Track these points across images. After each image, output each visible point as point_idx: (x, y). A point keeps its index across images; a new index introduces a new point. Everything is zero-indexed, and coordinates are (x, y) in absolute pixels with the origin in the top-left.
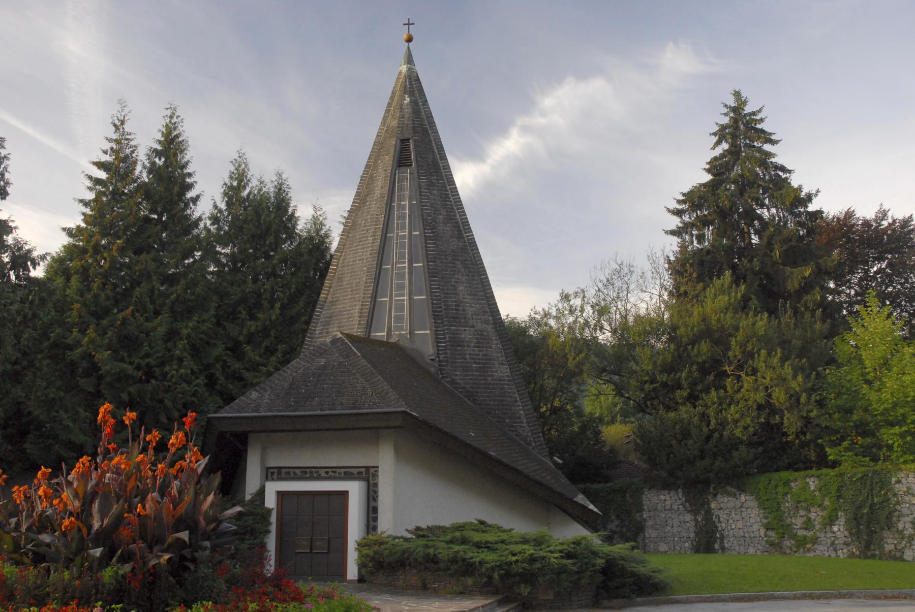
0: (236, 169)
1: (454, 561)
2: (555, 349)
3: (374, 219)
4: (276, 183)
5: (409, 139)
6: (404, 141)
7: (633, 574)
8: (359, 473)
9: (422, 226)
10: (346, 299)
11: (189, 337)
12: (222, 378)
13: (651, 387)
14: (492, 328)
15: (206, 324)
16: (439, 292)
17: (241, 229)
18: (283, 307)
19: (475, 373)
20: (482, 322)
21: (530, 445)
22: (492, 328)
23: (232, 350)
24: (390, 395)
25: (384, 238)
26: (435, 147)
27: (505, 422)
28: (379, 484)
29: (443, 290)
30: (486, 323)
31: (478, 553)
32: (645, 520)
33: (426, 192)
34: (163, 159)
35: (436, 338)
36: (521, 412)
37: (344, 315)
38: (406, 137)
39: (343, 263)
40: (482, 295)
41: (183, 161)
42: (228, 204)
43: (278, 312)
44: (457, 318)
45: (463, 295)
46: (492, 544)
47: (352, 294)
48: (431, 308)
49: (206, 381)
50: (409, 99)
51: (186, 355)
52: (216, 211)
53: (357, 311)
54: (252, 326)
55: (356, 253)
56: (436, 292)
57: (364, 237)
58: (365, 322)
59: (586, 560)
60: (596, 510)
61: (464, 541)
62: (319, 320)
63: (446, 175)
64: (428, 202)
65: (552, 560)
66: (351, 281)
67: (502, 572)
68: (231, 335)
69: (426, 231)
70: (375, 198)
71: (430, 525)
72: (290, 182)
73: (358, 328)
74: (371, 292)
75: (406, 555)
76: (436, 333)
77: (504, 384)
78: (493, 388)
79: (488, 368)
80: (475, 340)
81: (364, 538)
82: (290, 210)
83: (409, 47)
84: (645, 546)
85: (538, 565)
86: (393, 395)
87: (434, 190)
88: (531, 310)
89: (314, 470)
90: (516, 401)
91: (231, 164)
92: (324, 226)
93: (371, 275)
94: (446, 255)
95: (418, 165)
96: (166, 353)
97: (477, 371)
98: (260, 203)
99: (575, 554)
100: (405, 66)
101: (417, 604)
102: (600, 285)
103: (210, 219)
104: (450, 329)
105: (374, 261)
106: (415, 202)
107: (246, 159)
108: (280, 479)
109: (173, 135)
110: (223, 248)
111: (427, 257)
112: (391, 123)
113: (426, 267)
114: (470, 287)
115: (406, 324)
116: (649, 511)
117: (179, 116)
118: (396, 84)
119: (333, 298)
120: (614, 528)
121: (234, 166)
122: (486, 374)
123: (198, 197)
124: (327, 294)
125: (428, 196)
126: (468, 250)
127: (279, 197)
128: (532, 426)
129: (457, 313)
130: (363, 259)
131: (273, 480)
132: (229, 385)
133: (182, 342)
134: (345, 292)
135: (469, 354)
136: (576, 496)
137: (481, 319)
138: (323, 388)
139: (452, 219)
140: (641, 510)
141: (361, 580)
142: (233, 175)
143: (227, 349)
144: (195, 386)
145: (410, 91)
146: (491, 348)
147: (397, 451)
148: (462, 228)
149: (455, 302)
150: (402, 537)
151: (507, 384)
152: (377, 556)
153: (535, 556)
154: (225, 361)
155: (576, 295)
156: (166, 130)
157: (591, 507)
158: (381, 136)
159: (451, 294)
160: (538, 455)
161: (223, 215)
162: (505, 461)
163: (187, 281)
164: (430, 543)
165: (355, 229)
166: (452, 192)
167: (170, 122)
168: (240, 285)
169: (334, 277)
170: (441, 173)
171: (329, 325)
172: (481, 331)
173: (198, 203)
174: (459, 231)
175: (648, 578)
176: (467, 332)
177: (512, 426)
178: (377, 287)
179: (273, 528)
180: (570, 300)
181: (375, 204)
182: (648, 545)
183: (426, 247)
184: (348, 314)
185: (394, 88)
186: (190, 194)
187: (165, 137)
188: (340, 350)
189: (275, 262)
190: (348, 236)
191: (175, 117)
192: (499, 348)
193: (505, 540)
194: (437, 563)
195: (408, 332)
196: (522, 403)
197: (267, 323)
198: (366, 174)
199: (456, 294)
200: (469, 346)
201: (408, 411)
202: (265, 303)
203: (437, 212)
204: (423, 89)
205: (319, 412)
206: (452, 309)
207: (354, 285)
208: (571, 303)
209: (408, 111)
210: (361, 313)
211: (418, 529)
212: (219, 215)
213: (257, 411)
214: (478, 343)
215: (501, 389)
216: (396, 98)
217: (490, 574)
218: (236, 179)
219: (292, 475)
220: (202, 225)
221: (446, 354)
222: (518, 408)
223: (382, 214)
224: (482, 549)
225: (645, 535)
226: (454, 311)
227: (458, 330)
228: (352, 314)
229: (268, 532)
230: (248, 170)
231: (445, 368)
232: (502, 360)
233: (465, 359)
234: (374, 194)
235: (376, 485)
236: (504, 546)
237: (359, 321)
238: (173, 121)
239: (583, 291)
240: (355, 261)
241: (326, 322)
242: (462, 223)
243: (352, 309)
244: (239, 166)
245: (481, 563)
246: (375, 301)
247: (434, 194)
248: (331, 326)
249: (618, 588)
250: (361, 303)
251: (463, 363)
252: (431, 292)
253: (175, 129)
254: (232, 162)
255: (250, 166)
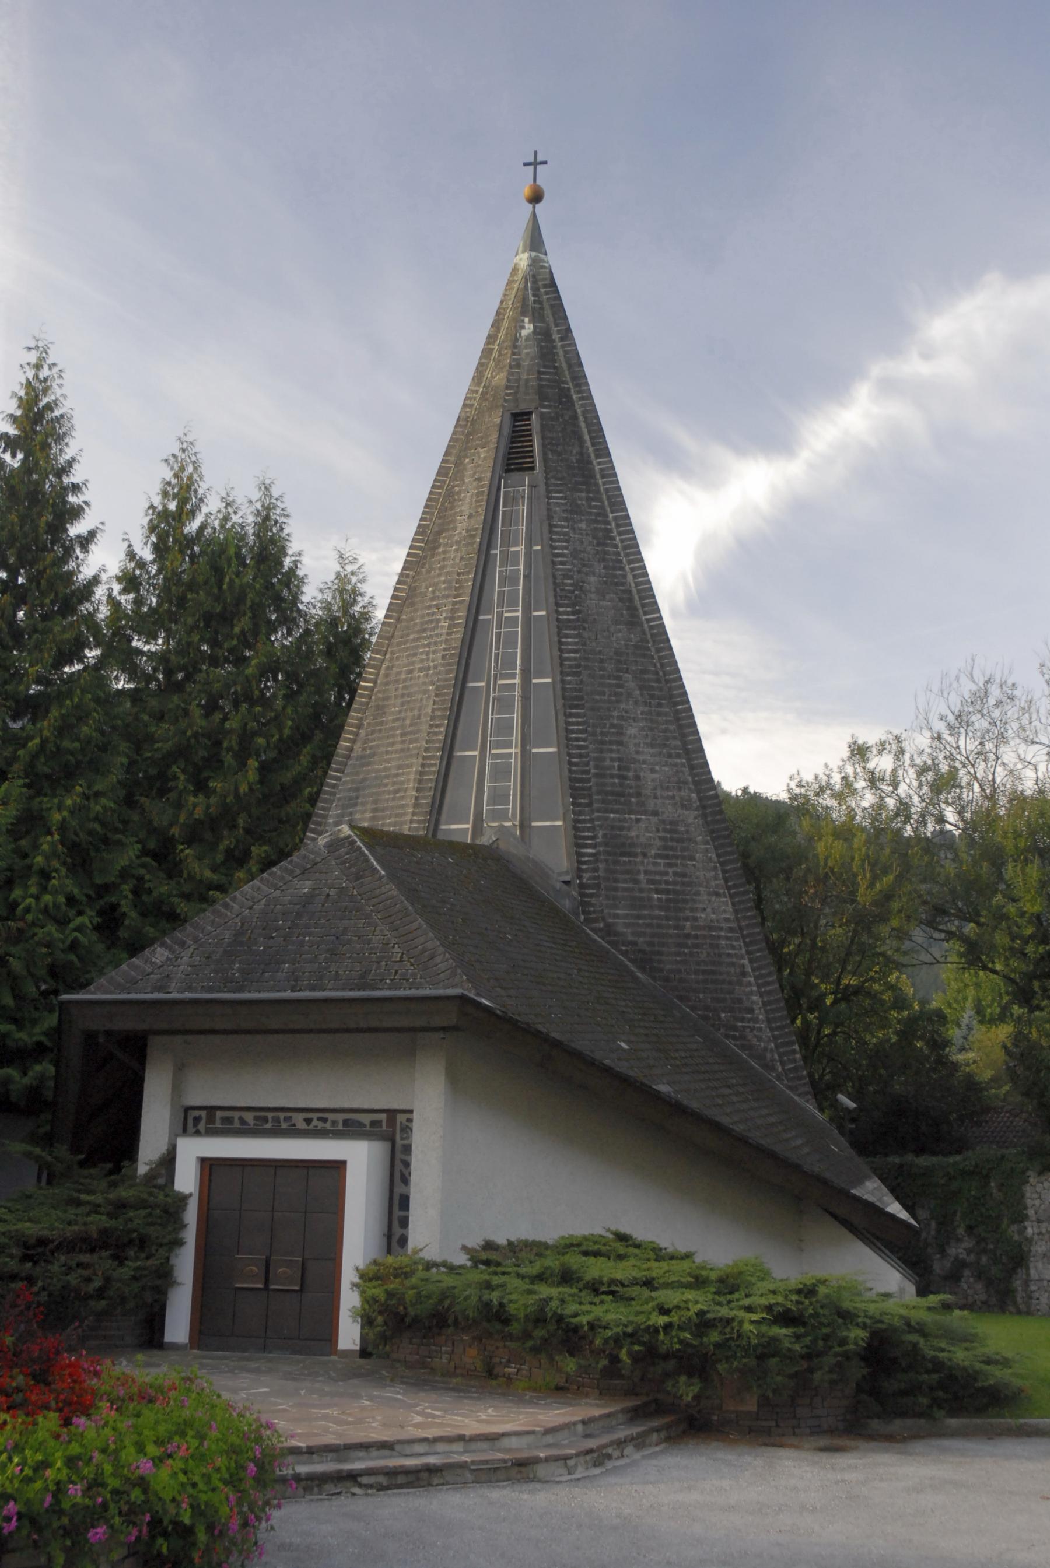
0: (176, 476)
1: (539, 1318)
2: (830, 863)
3: (454, 584)
4: (259, 506)
5: (530, 413)
6: (520, 417)
7: (938, 1366)
8: (375, 1123)
9: (552, 600)
10: (392, 752)
11: (63, 827)
12: (133, 914)
13: (1041, 949)
14: (695, 818)
15: (103, 801)
16: (584, 740)
17: (182, 601)
18: (264, 769)
19: (657, 912)
20: (675, 804)
21: (773, 1068)
22: (695, 818)
23: (155, 856)
24: (438, 959)
25: (471, 624)
26: (585, 431)
27: (720, 1018)
28: (413, 1147)
29: (594, 734)
30: (683, 806)
31: (591, 1303)
32: (1030, 1241)
33: (563, 527)
34: (20, 456)
35: (576, 837)
36: (755, 998)
37: (386, 785)
38: (523, 407)
39: (387, 675)
40: (676, 747)
41: (62, 460)
42: (157, 549)
43: (252, 776)
44: (622, 795)
45: (637, 745)
46: (623, 1285)
47: (403, 742)
48: (566, 773)
49: (97, 920)
50: (531, 326)
51: (56, 864)
52: (133, 564)
53: (412, 777)
54: (198, 806)
55: (415, 655)
56: (578, 740)
57: (431, 621)
58: (429, 801)
59: (825, 1330)
60: (903, 1215)
61: (567, 1277)
62: (334, 794)
63: (607, 490)
64: (566, 548)
65: (747, 1326)
66: (403, 715)
67: (637, 1348)
68: (155, 824)
69: (561, 609)
70: (456, 538)
71: (513, 1239)
72: (288, 503)
73: (414, 814)
74: (441, 737)
75: (447, 1303)
76: (576, 827)
77: (719, 937)
78: (697, 946)
79: (685, 901)
80: (659, 843)
81: (375, 1262)
82: (287, 562)
83: (534, 215)
84: (1031, 1298)
85: (715, 1337)
86: (444, 961)
87: (581, 521)
88: (791, 778)
89: (282, 1115)
90: (744, 974)
91: (165, 465)
92: (360, 594)
93: (444, 702)
94: (602, 661)
95: (547, 469)
96: (17, 860)
97: (660, 908)
98: (223, 548)
99: (802, 1315)
100: (526, 255)
101: (446, 1411)
102: (940, 727)
103: (119, 579)
104: (607, 819)
105: (448, 672)
106: (539, 548)
107: (195, 454)
108: (212, 1132)
109: (41, 404)
110: (147, 643)
111: (561, 665)
112: (493, 377)
113: (559, 686)
114: (651, 729)
115: (513, 807)
116: (1039, 1221)
117: (54, 364)
118: (505, 295)
119: (364, 749)
120: (963, 1256)
121: (172, 468)
122: (681, 915)
123: (92, 535)
124: (354, 741)
125: (566, 534)
126: (648, 649)
127: (265, 535)
128: (778, 1028)
129: (621, 785)
130: (429, 668)
131: (198, 1133)
132: (148, 928)
133: (49, 838)
134: (388, 737)
135: (646, 872)
136: (859, 1181)
137: (673, 797)
138: (303, 941)
139: (616, 584)
140: (1020, 1218)
141: (364, 1353)
142: (169, 489)
143: (145, 852)
144: (75, 930)
145: (534, 308)
146: (692, 858)
147: (453, 1079)
148: (637, 603)
149: (620, 760)
150: (444, 1264)
151: (727, 938)
152: (393, 1302)
153: (709, 1316)
154: (140, 879)
155: (882, 747)
156: (27, 394)
157: (895, 1208)
158: (471, 406)
159: (611, 743)
160: (788, 1092)
161: (148, 573)
162: (694, 1105)
163: (64, 711)
164: (496, 1280)
165: (413, 604)
166: (618, 526)
167: (36, 376)
168: (177, 720)
169: (368, 703)
170: (597, 485)
171: (356, 805)
172: (671, 823)
173: (92, 547)
174: (632, 609)
175: (973, 1376)
176: (642, 825)
177: (735, 1028)
178: (455, 728)
179: (190, 1235)
180: (868, 760)
181: (457, 550)
182: (1036, 1295)
183: (560, 643)
184: (394, 784)
185: (502, 302)
186: (76, 529)
187: (24, 409)
188: (344, 862)
189: (249, 671)
190: (398, 620)
191: (46, 367)
192: (710, 859)
193: (653, 1279)
194: (506, 1322)
195: (517, 823)
196: (756, 978)
197: (230, 799)
198: (439, 487)
199: (620, 743)
200: (645, 855)
201: (472, 995)
202: (228, 759)
203: (585, 569)
204: (562, 305)
205: (288, 995)
206: (612, 776)
207: (408, 722)
208: (871, 765)
209: (528, 351)
210: (420, 781)
211: (489, 1246)
212: (138, 572)
213: (159, 989)
214: (665, 848)
215: (711, 945)
216: (505, 324)
217: (615, 1352)
218: (175, 496)
219: (237, 1124)
220: (100, 592)
221: (596, 870)
222: (748, 989)
223: (469, 573)
224: (604, 1297)
225: (1028, 1275)
226: (616, 781)
227: (625, 820)
228: (402, 783)
229: (180, 1243)
230: (201, 477)
231: (593, 900)
232: (717, 886)
233: (636, 881)
234: (455, 529)
235: (407, 1149)
236: (646, 1293)
237: (417, 798)
238: (41, 376)
239: (898, 739)
240: (410, 672)
241: (350, 798)
242: (639, 591)
243: (403, 774)
244: (182, 469)
245: (592, 1326)
246: (450, 757)
247: (580, 529)
248: (359, 808)
249: (904, 1393)
250: (420, 760)
251: (631, 890)
252: (568, 739)
253: (46, 391)
254: (166, 461)
255: (204, 470)
